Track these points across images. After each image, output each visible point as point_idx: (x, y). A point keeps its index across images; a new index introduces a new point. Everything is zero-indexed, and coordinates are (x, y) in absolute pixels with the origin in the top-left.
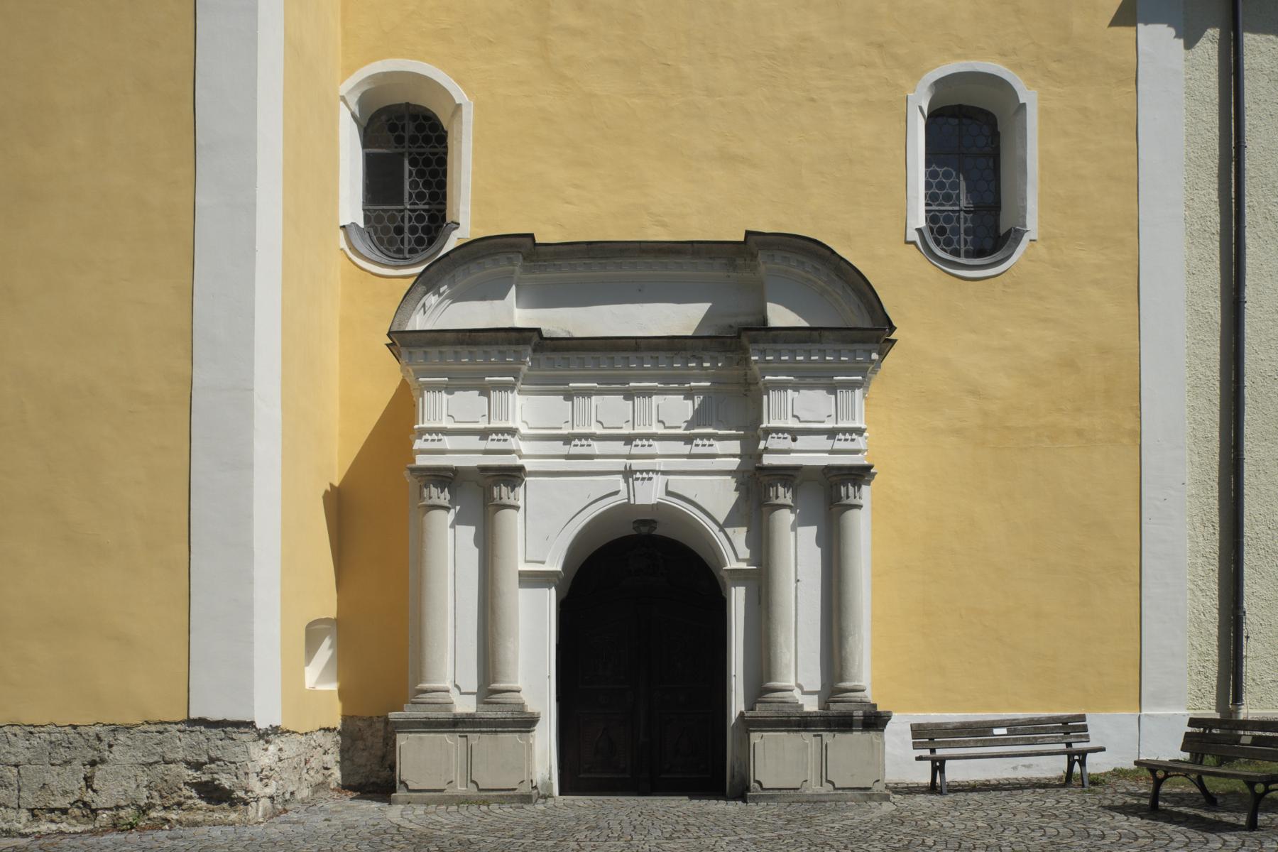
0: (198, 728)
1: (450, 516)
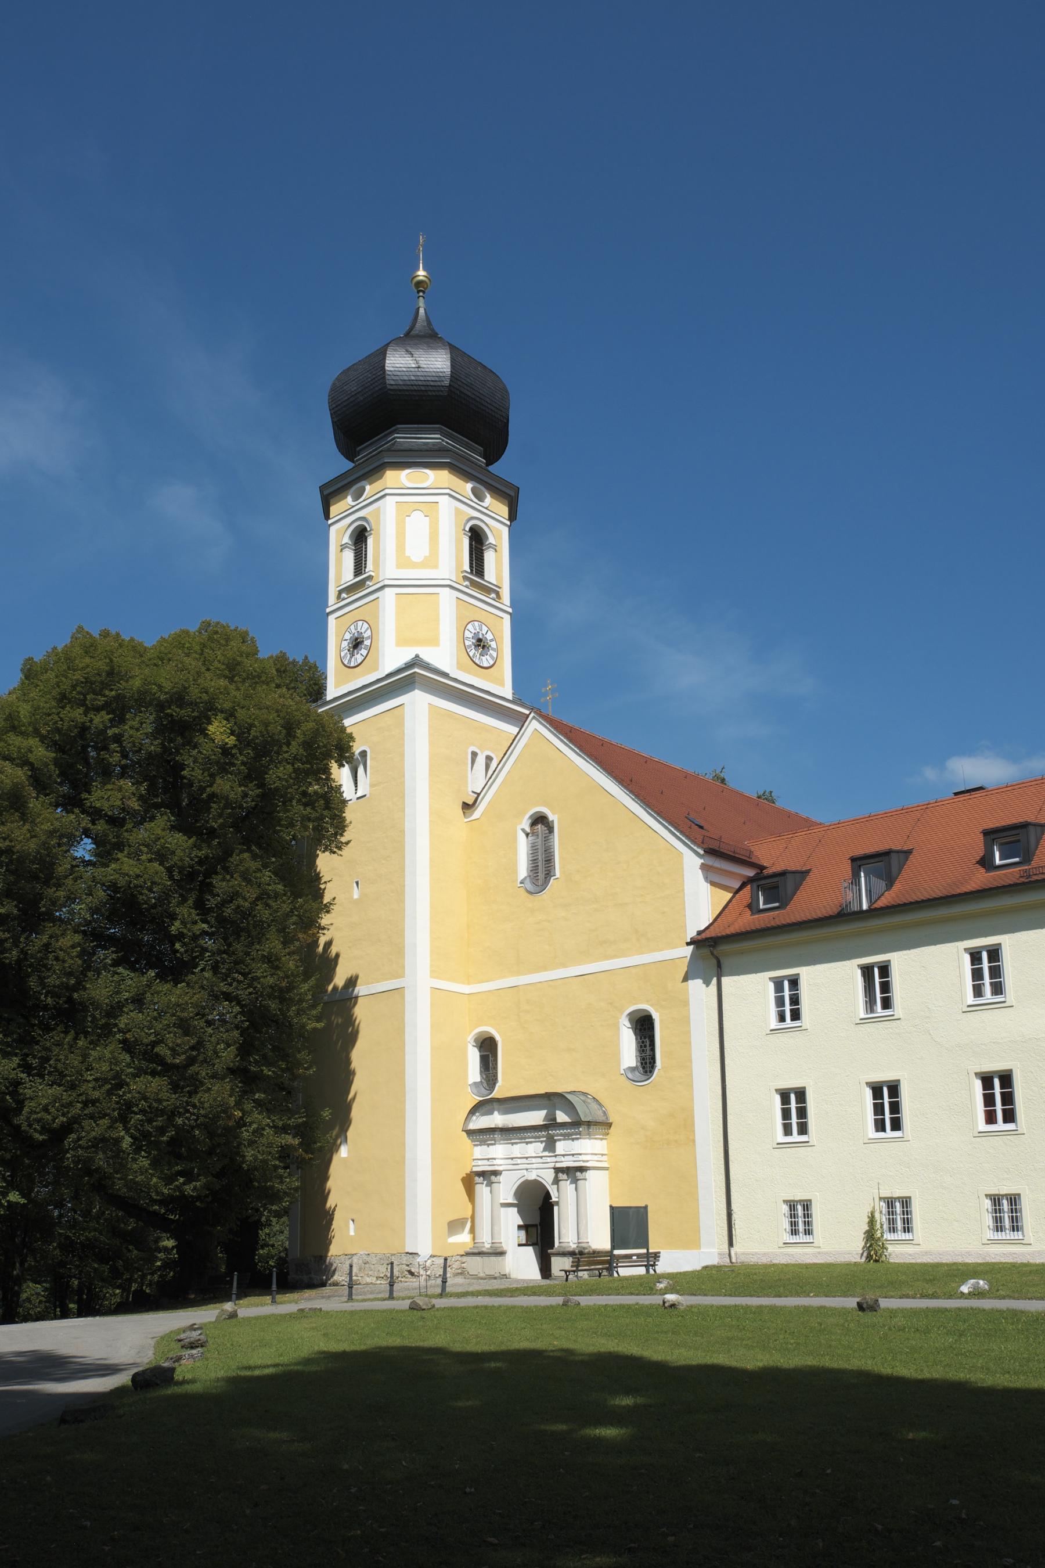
1: (569, 1182)
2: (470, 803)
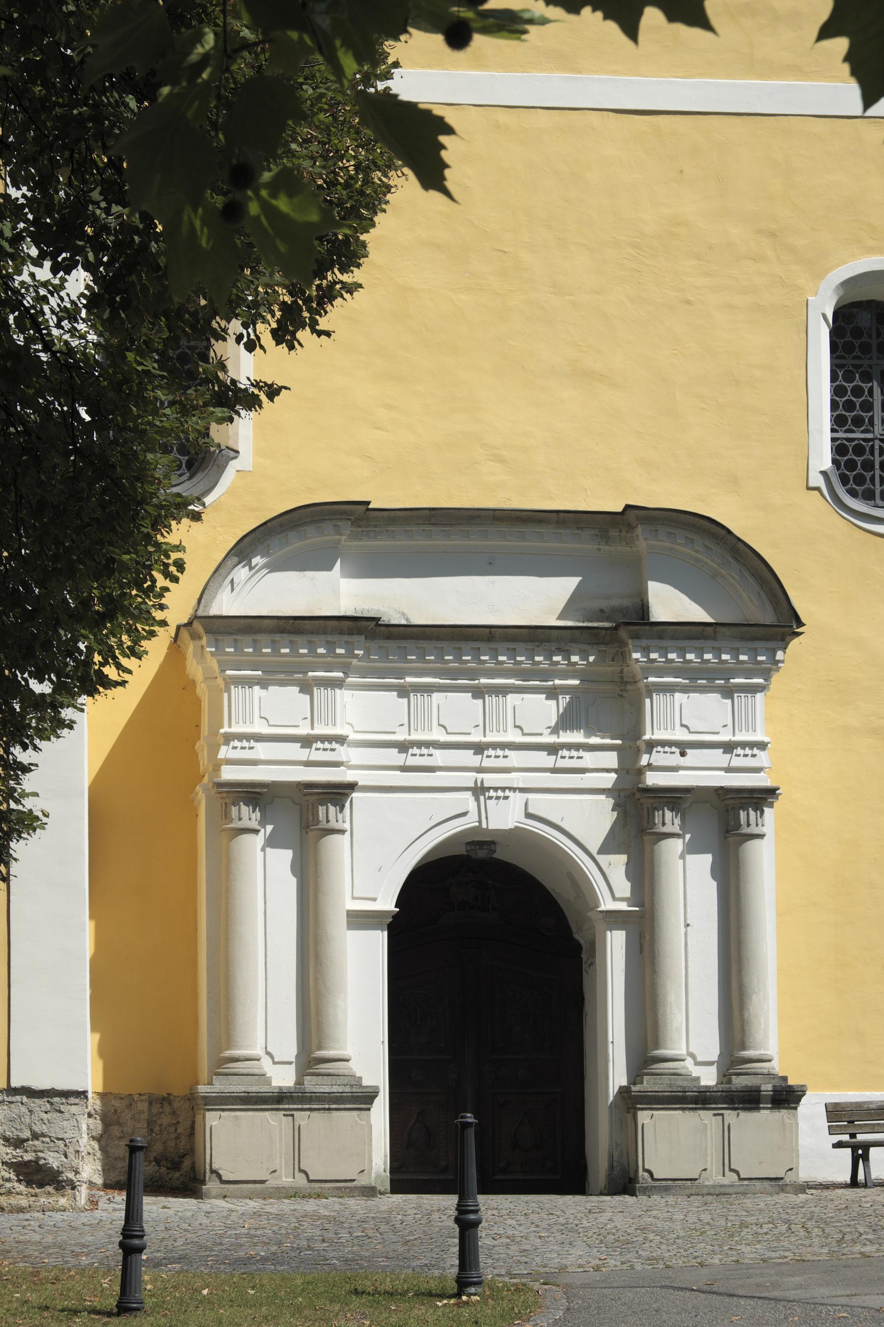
0: (18, 1098)
1: (259, 840)
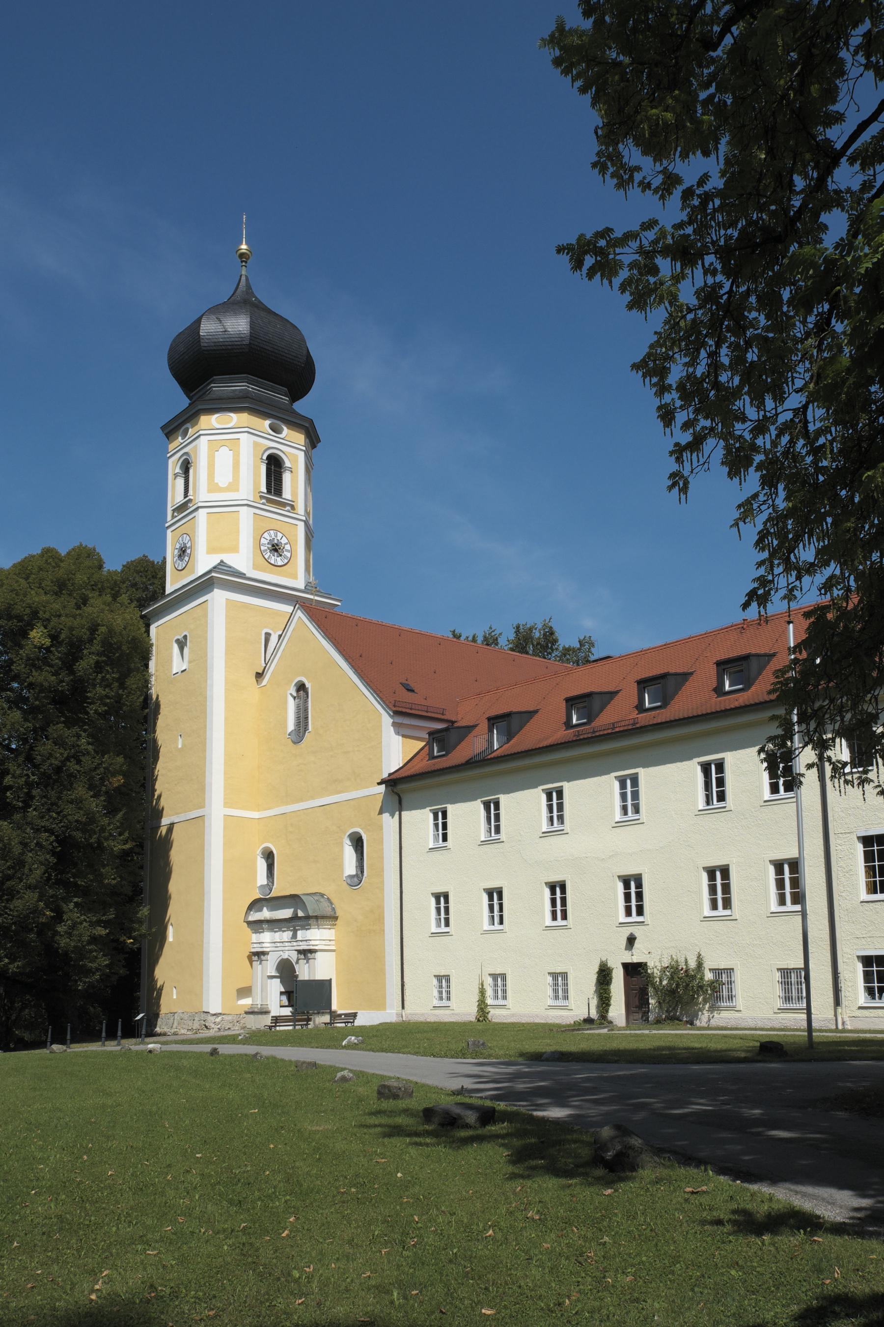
2: (260, 672)
